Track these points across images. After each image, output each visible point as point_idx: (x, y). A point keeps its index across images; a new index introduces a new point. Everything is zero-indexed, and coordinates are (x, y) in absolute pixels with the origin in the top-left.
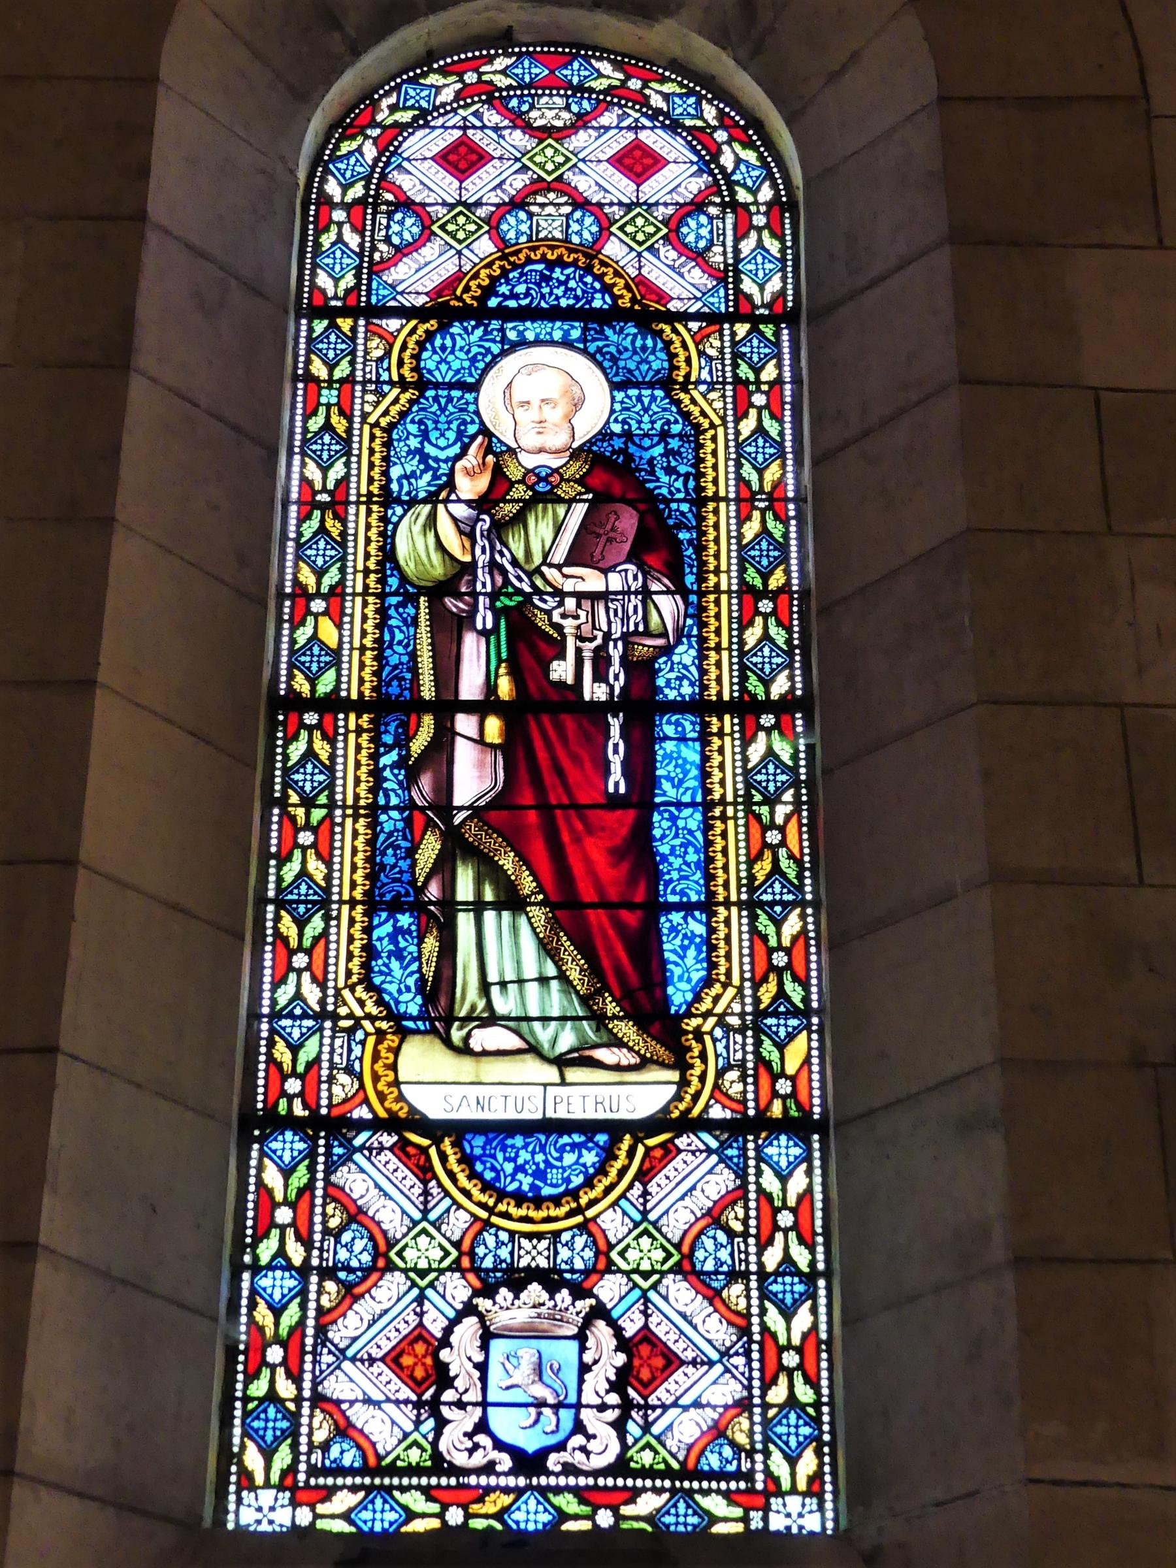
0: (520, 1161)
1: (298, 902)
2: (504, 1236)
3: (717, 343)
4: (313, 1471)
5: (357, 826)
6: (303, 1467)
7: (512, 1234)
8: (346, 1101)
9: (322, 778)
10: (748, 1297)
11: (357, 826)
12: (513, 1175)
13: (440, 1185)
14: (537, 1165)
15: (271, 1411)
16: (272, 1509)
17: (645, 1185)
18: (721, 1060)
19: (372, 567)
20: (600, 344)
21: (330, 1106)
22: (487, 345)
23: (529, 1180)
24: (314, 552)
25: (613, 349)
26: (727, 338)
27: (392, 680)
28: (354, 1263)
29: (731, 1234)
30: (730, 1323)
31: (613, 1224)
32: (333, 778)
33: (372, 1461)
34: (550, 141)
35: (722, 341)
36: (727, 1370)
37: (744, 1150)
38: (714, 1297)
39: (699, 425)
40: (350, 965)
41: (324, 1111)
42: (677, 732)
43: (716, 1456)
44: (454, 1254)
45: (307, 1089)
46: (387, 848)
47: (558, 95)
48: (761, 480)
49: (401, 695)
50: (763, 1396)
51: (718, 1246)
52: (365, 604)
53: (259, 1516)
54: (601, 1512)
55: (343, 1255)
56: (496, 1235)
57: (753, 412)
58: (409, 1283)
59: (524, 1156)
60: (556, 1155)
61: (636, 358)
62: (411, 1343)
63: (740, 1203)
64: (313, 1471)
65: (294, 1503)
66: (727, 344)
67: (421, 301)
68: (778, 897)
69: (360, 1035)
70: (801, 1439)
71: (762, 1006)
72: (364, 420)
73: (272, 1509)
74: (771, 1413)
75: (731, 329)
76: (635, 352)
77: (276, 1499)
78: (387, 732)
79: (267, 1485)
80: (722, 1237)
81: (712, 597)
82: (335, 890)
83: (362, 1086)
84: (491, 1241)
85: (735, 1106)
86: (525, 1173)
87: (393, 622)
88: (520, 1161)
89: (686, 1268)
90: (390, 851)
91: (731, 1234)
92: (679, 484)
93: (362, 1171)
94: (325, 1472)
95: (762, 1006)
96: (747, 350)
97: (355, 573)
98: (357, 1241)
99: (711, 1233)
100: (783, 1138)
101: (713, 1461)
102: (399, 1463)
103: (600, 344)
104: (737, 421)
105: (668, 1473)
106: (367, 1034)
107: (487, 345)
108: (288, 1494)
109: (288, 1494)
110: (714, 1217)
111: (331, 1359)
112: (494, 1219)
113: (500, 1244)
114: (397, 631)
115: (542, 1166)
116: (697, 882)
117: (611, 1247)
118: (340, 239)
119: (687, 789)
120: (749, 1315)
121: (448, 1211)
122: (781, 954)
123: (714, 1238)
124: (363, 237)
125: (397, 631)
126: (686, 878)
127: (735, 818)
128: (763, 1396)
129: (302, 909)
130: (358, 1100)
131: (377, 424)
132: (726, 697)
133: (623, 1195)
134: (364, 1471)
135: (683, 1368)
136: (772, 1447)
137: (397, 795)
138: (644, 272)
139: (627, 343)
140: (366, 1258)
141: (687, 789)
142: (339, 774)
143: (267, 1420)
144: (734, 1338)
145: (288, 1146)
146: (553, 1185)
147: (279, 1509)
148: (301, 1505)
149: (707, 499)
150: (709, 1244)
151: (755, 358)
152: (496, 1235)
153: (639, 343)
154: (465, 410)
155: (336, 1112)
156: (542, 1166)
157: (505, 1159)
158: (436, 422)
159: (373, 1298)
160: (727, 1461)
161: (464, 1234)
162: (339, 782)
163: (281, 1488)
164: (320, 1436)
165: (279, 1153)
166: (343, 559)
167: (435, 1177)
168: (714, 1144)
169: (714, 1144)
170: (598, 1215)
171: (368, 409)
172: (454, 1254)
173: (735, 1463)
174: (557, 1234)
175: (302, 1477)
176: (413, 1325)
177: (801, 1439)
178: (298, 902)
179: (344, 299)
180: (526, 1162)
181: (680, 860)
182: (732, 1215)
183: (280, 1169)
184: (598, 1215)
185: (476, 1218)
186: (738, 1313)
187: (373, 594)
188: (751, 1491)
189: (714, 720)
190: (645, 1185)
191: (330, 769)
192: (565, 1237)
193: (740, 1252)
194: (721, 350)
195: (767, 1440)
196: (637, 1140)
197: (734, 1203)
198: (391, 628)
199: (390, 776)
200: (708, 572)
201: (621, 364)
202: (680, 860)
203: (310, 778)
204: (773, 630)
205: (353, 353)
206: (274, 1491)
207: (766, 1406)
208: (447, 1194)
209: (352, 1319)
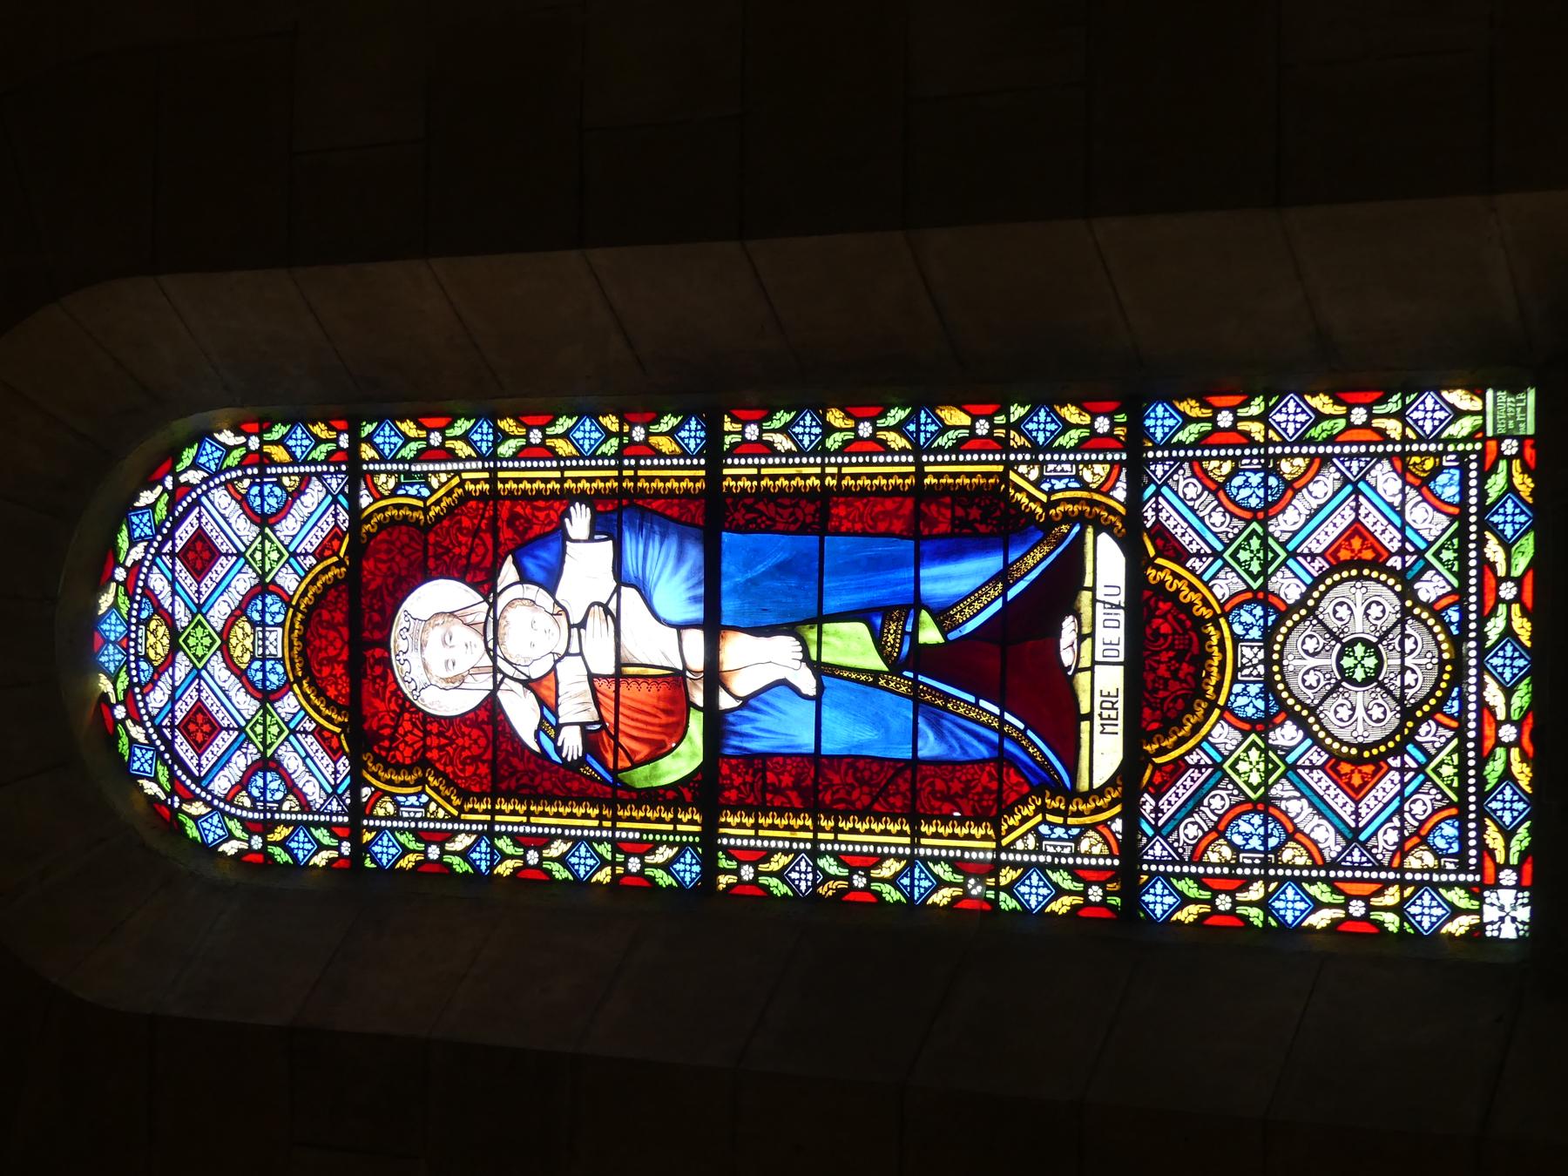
0: (1167, 675)
1: (912, 879)
2: (1238, 688)
3: (383, 477)
4: (1463, 867)
5: (685, 820)
6: (1462, 877)
7: (1234, 681)
8: (1106, 842)
9: (583, 849)
10: (1292, 456)
11: (685, 820)
12: (1182, 681)
13: (1189, 752)
14: (1171, 659)
15: (1414, 910)
16: (1502, 908)
17: (1190, 556)
18: (1071, 485)
19: (597, 811)
20: (385, 592)
21: (1112, 856)
22: (388, 695)
23: (1185, 665)
24: (688, 874)
25: (390, 580)
26: (377, 467)
27: (565, 787)
28: (1261, 831)
29: (1235, 472)
30: (1317, 473)
31: (1226, 586)
32: (582, 838)
33: (1453, 811)
34: (181, 640)
35: (380, 472)
36: (1363, 478)
37: (1156, 461)
38: (1292, 487)
39: (460, 497)
40: (978, 836)
41: (1116, 862)
42: (471, 764)
43: (1447, 489)
44: (1253, 737)
45: (864, 865)
46: (887, 802)
47: (136, 632)
48: (557, 436)
49: (904, 795)
50: (1394, 442)
51: (1247, 484)
52: (502, 812)
53: (1508, 919)
54: (1502, 594)
55: (1255, 843)
56: (1237, 695)
57: (449, 444)
58: (1283, 781)
59: (1162, 671)
60: (1162, 640)
61: (398, 559)
62: (1340, 776)
63: (1205, 464)
64: (1463, 867)
65: (1497, 885)
66: (383, 467)
67: (344, 765)
68: (922, 428)
69: (1044, 829)
70: (1034, 434)
71: (909, 446)
72: (454, 819)
73: (1502, 908)
74: (1411, 434)
75: (367, 463)
76: (392, 559)
77: (1492, 905)
78: (940, 809)
79: (1480, 912)
80: (1238, 481)
81: (500, 486)
82: (901, 850)
83: (1093, 827)
84: (1242, 701)
85: (1116, 471)
86: (1177, 670)
87: (513, 784)
88: (1167, 675)
89: (1267, 512)
90: (568, 784)
91: (1235, 472)
92: (541, 515)
93: (1375, 833)
94: (1462, 855)
95: (909, 446)
96: (212, 463)
97: (841, 842)
98: (1241, 830)
99: (1234, 491)
100: (1149, 423)
101: (1451, 493)
102: (1455, 784)
103: (385, 592)
104: (458, 459)
105: (1462, 533)
106: (1044, 822)
107: (388, 695)
108: (1486, 893)
109: (1486, 893)
110: (1218, 489)
111: (1356, 853)
112: (1221, 702)
113: (1245, 693)
114: (521, 782)
115: (1172, 654)
116: (866, 505)
117: (1249, 588)
118: (321, 847)
119: (777, 513)
120: (1312, 457)
121: (1213, 745)
122: (532, 435)
123: (1239, 488)
124: (661, 843)
125: (521, 782)
126: (861, 516)
127: (840, 466)
128: (1394, 442)
129: (906, 881)
130: (1105, 831)
131: (460, 809)
132: (726, 471)
133: (1199, 577)
134: (1462, 818)
135: (1361, 518)
136: (1445, 435)
137: (838, 791)
138: (311, 549)
139: (383, 567)
140: (1257, 820)
141: (777, 513)
142: (579, 833)
143: (691, 865)
144: (1333, 469)
145: (1426, 911)
146: (1190, 644)
147: (1502, 902)
148: (1497, 879)
149: (494, 489)
150: (1244, 493)
151: (218, 454)
152: (1237, 695)
153: (383, 556)
154: (752, 785)
155: (1116, 851)
156: (1172, 654)
157: (1165, 689)
158: (463, 748)
159: (1298, 815)
160: (1451, 479)
161: (1236, 728)
162: (586, 833)
163: (1482, 900)
164: (1430, 861)
165: (1297, 913)
166: (590, 840)
167: (1182, 757)
168: (1152, 488)
169: (1152, 488)
170: (1218, 601)
171: (1020, 845)
172: (1253, 737)
173: (1452, 471)
174: (1236, 640)
175: (1470, 878)
176: (1322, 774)
177: (1034, 434)
178: (912, 879)
179: (341, 840)
180: (1168, 669)
181: (844, 522)
182: (1217, 472)
183: (1313, 911)
184: (1218, 601)
185: (1221, 717)
186: (1309, 467)
187: (493, 806)
188: (1482, 455)
189: (725, 483)
190: (1190, 556)
191: (576, 841)
192: (1238, 629)
193: (1250, 464)
194: (390, 473)
195: (1437, 440)
196: (1151, 563)
197: (1205, 471)
198: (835, 802)
199: (506, 783)
200: (562, 489)
201: (404, 573)
202: (844, 522)
203: (481, 856)
204: (414, 446)
205: (392, 830)
206: (1485, 907)
207: (1405, 440)
208: (1198, 745)
209: (308, 789)
